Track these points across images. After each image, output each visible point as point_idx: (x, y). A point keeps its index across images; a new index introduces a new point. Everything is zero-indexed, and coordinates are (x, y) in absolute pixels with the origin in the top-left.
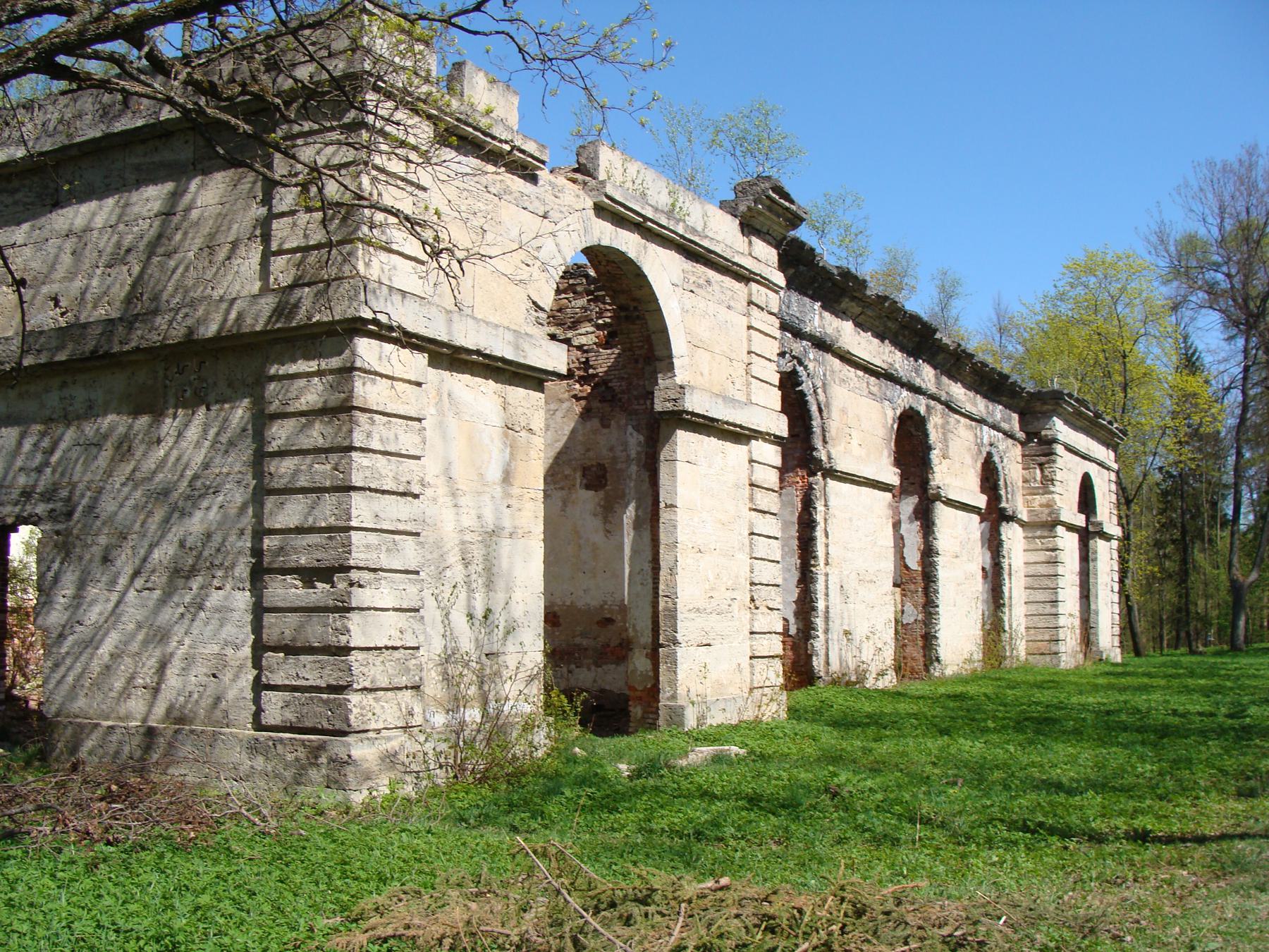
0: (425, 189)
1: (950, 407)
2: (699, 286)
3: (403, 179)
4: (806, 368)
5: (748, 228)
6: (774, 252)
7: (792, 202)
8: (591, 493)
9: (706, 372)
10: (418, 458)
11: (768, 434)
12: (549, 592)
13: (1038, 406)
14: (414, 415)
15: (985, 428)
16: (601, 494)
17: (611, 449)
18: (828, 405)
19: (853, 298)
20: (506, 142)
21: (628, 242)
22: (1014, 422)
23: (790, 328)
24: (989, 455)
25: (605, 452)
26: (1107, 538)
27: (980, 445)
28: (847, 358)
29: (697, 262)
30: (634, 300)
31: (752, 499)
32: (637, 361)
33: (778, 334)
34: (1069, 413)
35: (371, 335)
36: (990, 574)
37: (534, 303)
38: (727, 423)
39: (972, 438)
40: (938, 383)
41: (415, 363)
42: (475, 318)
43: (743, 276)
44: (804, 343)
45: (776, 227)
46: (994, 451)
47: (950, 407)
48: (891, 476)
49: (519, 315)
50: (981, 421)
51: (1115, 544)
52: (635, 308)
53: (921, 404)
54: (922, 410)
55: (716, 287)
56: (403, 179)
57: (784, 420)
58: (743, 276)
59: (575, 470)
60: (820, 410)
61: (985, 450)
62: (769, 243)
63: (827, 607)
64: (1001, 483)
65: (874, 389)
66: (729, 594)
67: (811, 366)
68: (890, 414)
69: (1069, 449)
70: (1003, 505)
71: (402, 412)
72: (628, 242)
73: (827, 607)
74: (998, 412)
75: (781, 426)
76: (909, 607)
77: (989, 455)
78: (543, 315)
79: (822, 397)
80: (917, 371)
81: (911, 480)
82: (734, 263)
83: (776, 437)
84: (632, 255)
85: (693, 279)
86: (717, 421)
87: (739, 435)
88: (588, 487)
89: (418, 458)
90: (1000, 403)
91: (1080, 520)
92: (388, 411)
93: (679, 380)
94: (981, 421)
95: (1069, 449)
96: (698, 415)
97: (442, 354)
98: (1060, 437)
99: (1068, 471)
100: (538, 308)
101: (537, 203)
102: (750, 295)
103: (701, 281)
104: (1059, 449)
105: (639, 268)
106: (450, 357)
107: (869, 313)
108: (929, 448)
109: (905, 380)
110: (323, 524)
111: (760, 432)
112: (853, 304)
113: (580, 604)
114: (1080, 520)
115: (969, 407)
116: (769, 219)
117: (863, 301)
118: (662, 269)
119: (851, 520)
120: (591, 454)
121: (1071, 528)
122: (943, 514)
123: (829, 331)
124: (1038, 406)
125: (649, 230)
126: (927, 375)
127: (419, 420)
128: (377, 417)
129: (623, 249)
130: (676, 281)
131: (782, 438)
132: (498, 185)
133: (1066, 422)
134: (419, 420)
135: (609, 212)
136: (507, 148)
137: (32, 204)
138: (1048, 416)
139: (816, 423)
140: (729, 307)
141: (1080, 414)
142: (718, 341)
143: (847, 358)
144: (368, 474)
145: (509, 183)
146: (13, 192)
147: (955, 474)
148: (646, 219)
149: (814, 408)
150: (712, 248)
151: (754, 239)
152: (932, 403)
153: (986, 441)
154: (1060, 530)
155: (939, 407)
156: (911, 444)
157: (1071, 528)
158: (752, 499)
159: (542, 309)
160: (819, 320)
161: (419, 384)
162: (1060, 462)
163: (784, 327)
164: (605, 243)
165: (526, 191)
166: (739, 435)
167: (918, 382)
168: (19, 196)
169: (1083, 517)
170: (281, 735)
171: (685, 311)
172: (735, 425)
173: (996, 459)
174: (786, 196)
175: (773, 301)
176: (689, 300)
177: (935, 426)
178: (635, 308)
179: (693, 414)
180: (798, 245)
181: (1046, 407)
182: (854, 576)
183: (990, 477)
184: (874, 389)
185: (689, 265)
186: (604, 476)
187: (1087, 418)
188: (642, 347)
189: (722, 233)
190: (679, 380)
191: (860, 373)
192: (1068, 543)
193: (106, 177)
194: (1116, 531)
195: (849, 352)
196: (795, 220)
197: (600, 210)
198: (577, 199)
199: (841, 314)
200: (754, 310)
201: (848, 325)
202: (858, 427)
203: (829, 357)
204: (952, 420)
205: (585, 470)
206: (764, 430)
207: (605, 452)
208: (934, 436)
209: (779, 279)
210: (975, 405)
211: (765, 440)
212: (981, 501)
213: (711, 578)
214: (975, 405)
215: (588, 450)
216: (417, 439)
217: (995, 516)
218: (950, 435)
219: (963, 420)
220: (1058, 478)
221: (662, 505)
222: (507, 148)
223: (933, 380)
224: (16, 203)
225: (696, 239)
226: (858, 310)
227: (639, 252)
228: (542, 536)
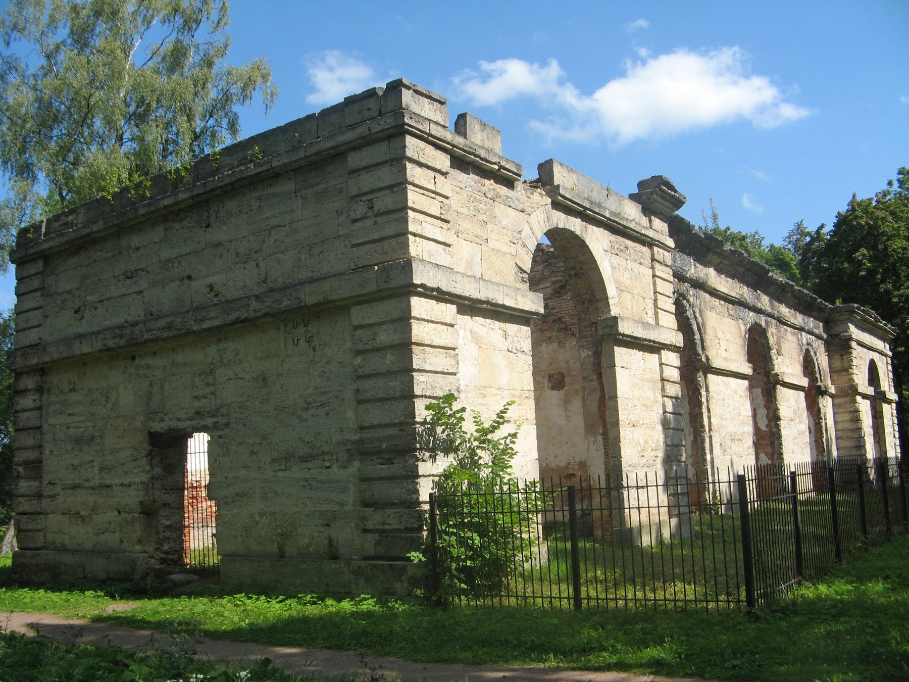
0: (447, 198)
1: (781, 321)
2: (621, 251)
3: (434, 192)
4: (688, 301)
5: (648, 211)
6: (666, 225)
7: (676, 191)
8: (555, 392)
9: (629, 307)
10: (455, 374)
11: (671, 345)
12: (540, 459)
13: (837, 317)
14: (450, 346)
15: (804, 333)
16: (562, 392)
17: (567, 362)
18: (703, 324)
19: (715, 253)
20: (495, 164)
21: (575, 225)
22: (819, 328)
23: (679, 276)
24: (807, 351)
25: (563, 365)
26: (889, 402)
27: (801, 346)
28: (714, 293)
29: (618, 235)
30: (580, 262)
31: (663, 389)
32: (583, 303)
33: (672, 279)
34: (858, 320)
35: (420, 295)
36: (813, 431)
37: (520, 268)
38: (645, 340)
39: (795, 340)
40: (772, 305)
41: (450, 310)
42: (484, 280)
43: (649, 243)
44: (686, 284)
45: (666, 209)
46: (810, 348)
47: (781, 321)
48: (747, 369)
49: (511, 275)
50: (801, 329)
51: (894, 405)
52: (581, 268)
53: (762, 320)
54: (763, 324)
55: (631, 251)
56: (434, 192)
57: (680, 335)
58: (649, 243)
59: (543, 377)
60: (699, 329)
61: (804, 348)
62: (662, 220)
63: (712, 459)
64: (817, 369)
65: (732, 312)
66: (653, 453)
67: (691, 299)
68: (743, 328)
69: (860, 344)
70: (819, 383)
71: (442, 344)
72: (575, 225)
73: (712, 459)
74: (811, 323)
75: (678, 339)
76: (762, 456)
77: (807, 351)
78: (526, 276)
79: (700, 319)
80: (758, 298)
81: (758, 371)
82: (642, 234)
83: (675, 347)
84: (578, 233)
85: (617, 246)
86: (639, 339)
87: (653, 347)
88: (553, 388)
89: (455, 374)
90: (811, 316)
91: (871, 391)
92: (434, 344)
93: (613, 313)
94: (801, 329)
95: (860, 344)
96: (627, 336)
97: (465, 305)
98: (854, 336)
99: (860, 360)
100: (522, 270)
101: (517, 203)
102: (653, 254)
103: (622, 248)
104: (854, 344)
105: (584, 241)
106: (470, 307)
107: (726, 262)
108: (770, 349)
109: (751, 304)
110: (396, 421)
111: (666, 345)
112: (715, 257)
113: (552, 465)
114: (871, 391)
115: (793, 320)
116: (660, 203)
117: (721, 254)
118: (598, 241)
119: (723, 400)
120: (553, 366)
121: (865, 396)
122: (783, 393)
123: (702, 275)
124: (837, 317)
125: (588, 216)
126: (764, 301)
127: (454, 349)
128: (427, 349)
129: (573, 229)
130: (606, 248)
131: (680, 348)
132: (492, 192)
133: (857, 327)
134: (454, 349)
135: (561, 205)
136: (496, 167)
137: (193, 227)
138: (845, 322)
139: (697, 337)
140: (640, 264)
141: (865, 320)
142: (634, 286)
143: (714, 293)
144: (424, 386)
145: (498, 190)
146: (181, 220)
147: (788, 366)
148: (586, 209)
149: (695, 327)
150: (628, 225)
151: (653, 217)
152: (769, 319)
153: (804, 342)
154: (859, 398)
155: (774, 321)
156: (758, 348)
157: (865, 396)
158: (663, 389)
159: (525, 272)
160: (694, 270)
161: (452, 326)
162: (854, 354)
163: (675, 275)
164: (561, 226)
165: (510, 195)
166: (653, 347)
167: (759, 305)
168: (185, 223)
169: (872, 389)
170: (375, 562)
171: (613, 268)
172: (650, 341)
173: (812, 354)
174: (672, 188)
175: (668, 257)
176: (616, 260)
177: (772, 334)
178: (581, 268)
179: (623, 335)
180: (681, 220)
181: (842, 317)
182: (728, 437)
183: (808, 366)
184: (732, 312)
185: (613, 238)
186: (563, 380)
187: (870, 323)
188: (586, 293)
189: (632, 214)
190: (613, 313)
191: (722, 302)
192: (864, 407)
193: (239, 206)
194: (893, 396)
195: (715, 289)
196: (679, 203)
197: (556, 205)
198: (540, 199)
199: (706, 264)
200: (657, 266)
201: (711, 271)
202: (725, 341)
203: (702, 293)
204: (782, 330)
205: (550, 377)
206: (668, 343)
207: (563, 365)
208: (772, 341)
209: (671, 243)
210: (796, 318)
211: (669, 350)
212: (804, 382)
213: (642, 443)
214: (796, 318)
215: (551, 364)
216: (453, 362)
217: (813, 394)
218: (782, 340)
219: (789, 329)
220: (854, 363)
221: (607, 397)
222: (496, 167)
223: (768, 304)
224: (183, 228)
225: (618, 220)
226: (718, 261)
227: (582, 231)
228: (535, 422)
